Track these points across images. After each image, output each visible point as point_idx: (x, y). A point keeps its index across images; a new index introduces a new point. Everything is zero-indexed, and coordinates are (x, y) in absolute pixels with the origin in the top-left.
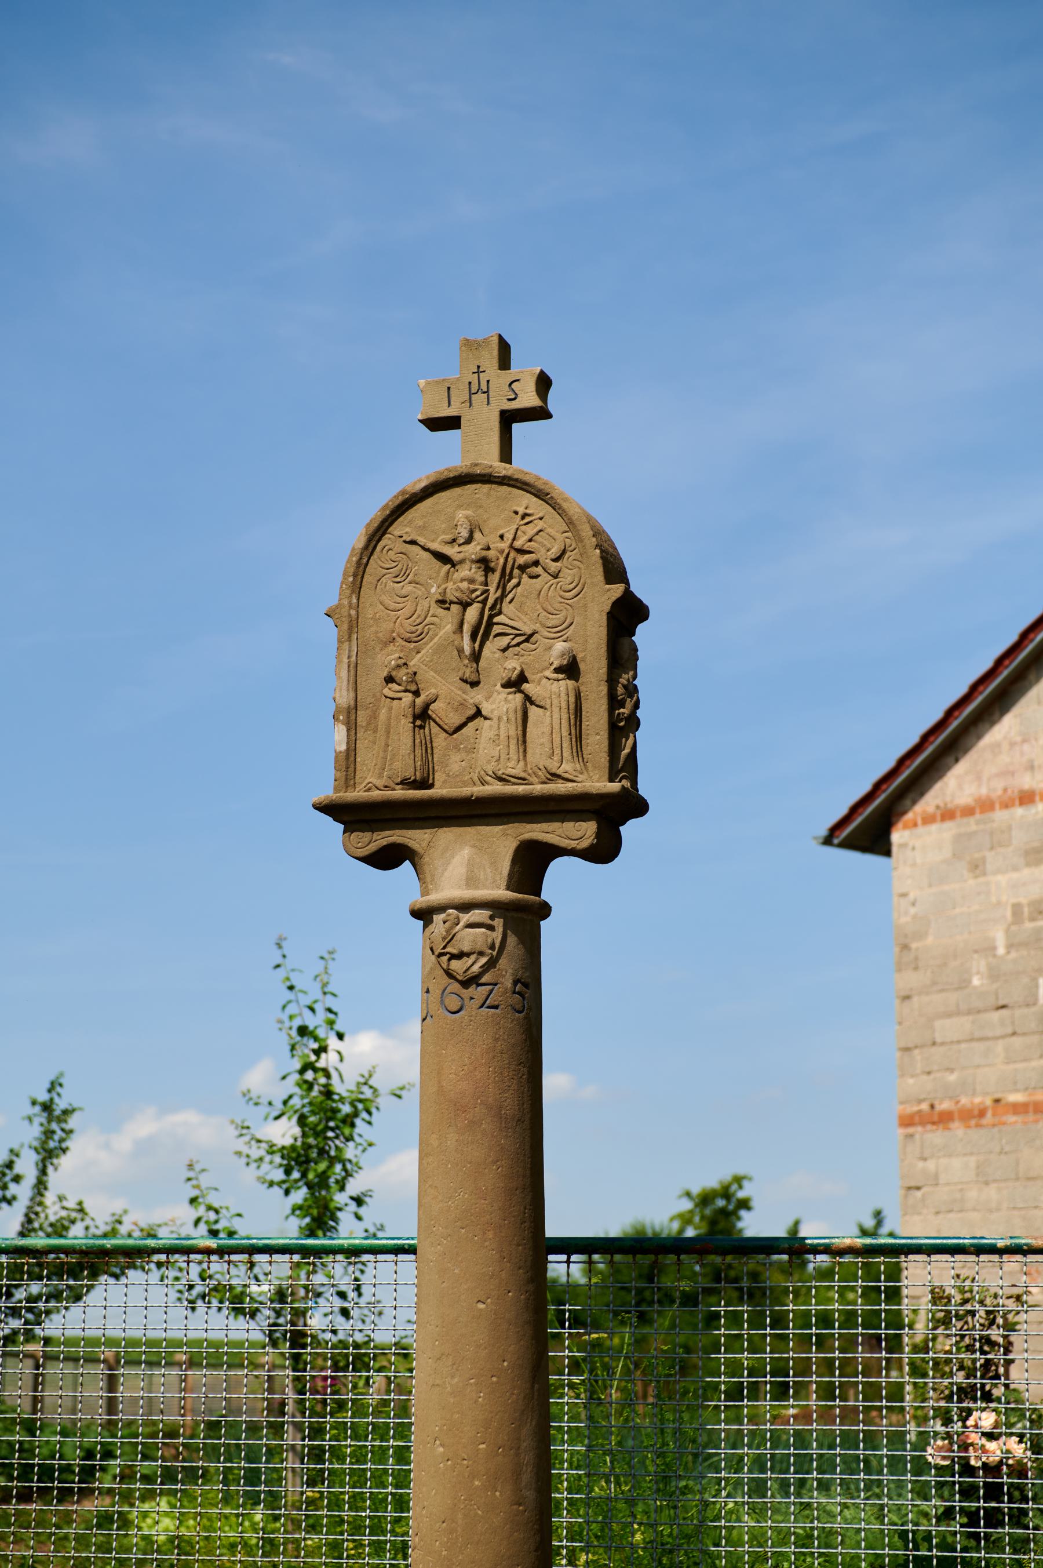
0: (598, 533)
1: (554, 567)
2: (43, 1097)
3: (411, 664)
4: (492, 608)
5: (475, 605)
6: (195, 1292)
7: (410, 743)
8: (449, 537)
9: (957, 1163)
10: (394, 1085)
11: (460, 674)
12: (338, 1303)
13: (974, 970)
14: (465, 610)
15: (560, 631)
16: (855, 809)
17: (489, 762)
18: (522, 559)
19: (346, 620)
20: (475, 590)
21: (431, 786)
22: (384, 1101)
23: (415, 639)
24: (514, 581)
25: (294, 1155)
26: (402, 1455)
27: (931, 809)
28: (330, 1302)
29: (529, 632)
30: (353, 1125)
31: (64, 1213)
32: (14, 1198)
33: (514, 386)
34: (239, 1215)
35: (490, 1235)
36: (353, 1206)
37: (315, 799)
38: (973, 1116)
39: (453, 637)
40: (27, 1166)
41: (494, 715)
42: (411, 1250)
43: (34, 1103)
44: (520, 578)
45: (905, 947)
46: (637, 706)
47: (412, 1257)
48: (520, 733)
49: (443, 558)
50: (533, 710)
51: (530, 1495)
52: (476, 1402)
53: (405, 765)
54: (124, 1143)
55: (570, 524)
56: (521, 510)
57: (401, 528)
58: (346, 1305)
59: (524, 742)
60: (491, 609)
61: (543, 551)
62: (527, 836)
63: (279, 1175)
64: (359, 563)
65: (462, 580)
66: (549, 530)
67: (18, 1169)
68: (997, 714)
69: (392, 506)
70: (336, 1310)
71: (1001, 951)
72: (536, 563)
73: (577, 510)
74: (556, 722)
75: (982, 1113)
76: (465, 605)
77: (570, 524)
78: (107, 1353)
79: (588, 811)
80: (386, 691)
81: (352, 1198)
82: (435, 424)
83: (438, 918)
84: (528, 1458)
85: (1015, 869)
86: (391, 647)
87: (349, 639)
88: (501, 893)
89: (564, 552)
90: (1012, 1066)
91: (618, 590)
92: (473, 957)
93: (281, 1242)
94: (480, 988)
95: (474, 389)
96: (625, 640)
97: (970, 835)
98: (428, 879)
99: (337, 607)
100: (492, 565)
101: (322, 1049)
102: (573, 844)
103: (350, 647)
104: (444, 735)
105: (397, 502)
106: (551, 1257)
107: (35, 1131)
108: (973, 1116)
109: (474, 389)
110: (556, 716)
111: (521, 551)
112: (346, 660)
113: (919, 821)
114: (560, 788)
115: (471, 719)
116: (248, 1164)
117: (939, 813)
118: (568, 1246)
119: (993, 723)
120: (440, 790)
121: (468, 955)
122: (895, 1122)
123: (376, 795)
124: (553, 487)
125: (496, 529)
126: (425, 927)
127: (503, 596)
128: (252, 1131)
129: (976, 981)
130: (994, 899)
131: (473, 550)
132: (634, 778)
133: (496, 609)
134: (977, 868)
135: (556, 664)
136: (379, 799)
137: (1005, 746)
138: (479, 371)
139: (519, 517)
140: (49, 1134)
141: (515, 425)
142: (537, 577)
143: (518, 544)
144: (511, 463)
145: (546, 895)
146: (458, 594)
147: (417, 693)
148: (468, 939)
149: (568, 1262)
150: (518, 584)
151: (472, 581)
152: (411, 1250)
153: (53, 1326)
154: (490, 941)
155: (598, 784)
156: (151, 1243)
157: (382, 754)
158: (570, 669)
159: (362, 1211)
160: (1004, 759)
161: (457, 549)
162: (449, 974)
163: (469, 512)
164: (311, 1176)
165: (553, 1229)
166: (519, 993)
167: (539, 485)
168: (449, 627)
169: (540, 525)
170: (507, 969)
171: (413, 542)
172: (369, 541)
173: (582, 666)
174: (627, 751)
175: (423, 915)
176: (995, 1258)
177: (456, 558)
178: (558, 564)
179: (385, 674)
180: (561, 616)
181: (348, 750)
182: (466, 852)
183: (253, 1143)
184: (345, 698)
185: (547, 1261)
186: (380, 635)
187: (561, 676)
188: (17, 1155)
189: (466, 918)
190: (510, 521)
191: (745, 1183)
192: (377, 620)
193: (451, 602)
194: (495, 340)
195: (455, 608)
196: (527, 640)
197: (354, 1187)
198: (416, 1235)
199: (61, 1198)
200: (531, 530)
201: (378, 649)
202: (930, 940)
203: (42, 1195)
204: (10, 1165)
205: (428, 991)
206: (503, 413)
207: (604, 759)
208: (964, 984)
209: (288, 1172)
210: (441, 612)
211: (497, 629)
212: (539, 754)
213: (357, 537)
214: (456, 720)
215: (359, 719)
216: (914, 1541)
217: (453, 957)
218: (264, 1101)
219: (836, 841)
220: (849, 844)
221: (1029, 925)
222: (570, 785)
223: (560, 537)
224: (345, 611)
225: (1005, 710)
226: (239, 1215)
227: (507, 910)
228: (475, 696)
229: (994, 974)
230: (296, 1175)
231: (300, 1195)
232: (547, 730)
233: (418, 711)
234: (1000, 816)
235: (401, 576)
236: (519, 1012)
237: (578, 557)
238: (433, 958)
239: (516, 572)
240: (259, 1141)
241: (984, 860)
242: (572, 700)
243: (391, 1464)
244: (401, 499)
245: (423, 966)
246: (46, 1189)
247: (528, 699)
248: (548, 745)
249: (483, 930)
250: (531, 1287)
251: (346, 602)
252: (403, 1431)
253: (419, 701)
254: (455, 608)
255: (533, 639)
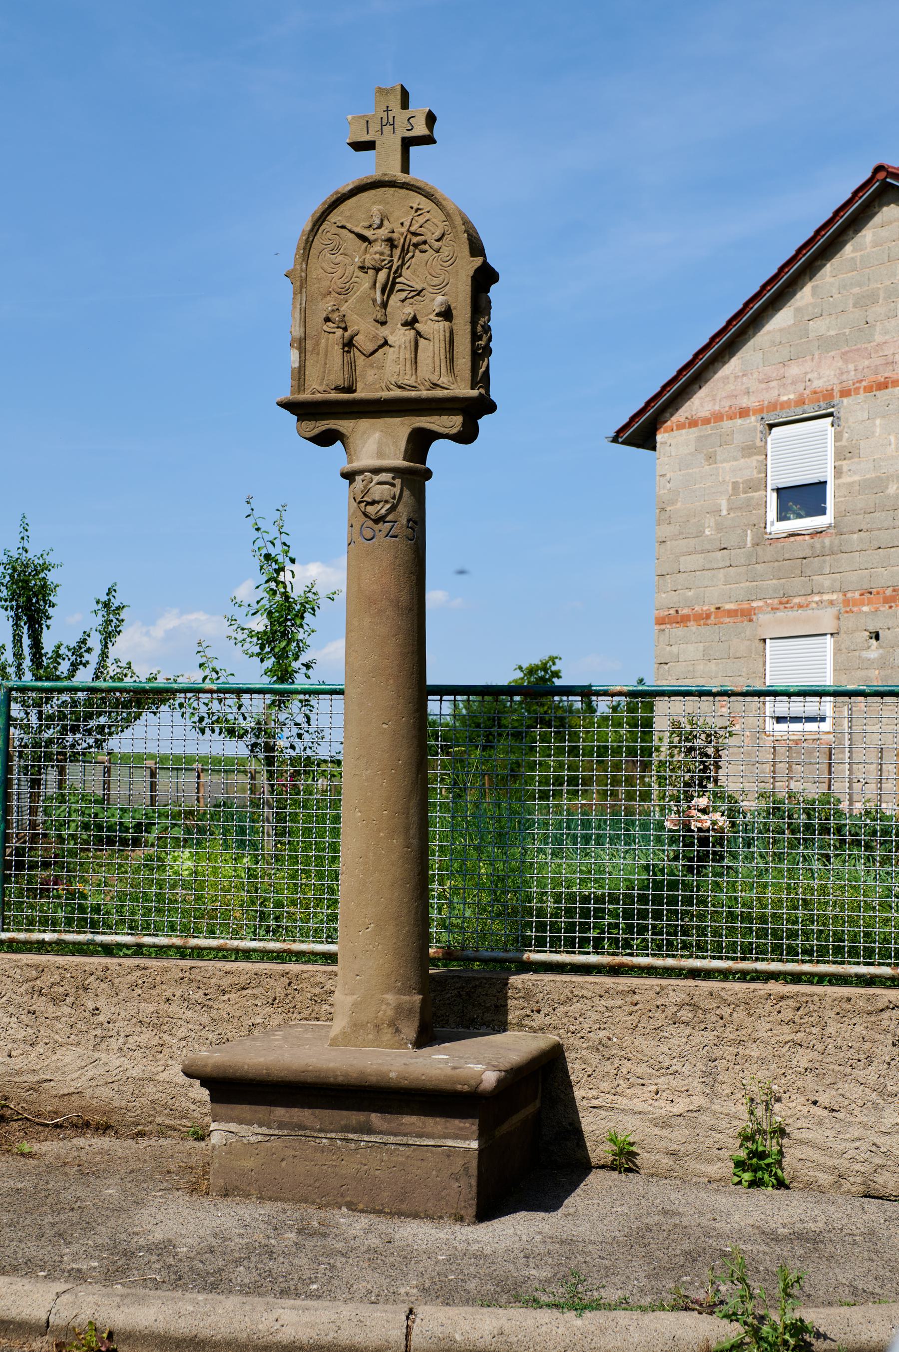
0: (466, 222)
1: (436, 245)
2: (104, 598)
3: (342, 309)
4: (395, 272)
5: (384, 270)
6: (204, 724)
7: (341, 362)
8: (367, 224)
9: (691, 647)
10: (329, 592)
11: (374, 316)
12: (295, 731)
13: (707, 525)
14: (377, 273)
15: (440, 288)
16: (633, 419)
17: (392, 375)
18: (415, 240)
19: (298, 279)
20: (384, 260)
21: (355, 391)
22: (323, 602)
23: (345, 292)
24: (410, 254)
25: (265, 638)
26: (337, 819)
27: (682, 419)
28: (290, 732)
29: (420, 289)
30: (302, 618)
31: (119, 670)
32: (88, 662)
33: (411, 120)
34: (233, 675)
35: (391, 681)
36: (304, 669)
37: (278, 399)
38: (703, 618)
39: (369, 291)
40: (95, 642)
41: (397, 344)
42: (341, 692)
43: (98, 602)
44: (414, 252)
45: (663, 509)
46: (490, 339)
47: (341, 697)
48: (413, 356)
49: (363, 238)
50: (422, 342)
51: (415, 842)
52: (381, 785)
53: (337, 377)
54: (158, 632)
55: (448, 215)
56: (415, 206)
57: (335, 217)
58: (300, 731)
59: (416, 362)
60: (394, 273)
61: (429, 234)
62: (417, 425)
63: (257, 649)
64: (307, 241)
65: (376, 253)
66: (434, 220)
67: (90, 644)
68: (727, 357)
69: (329, 202)
70: (295, 735)
71: (724, 512)
72: (425, 242)
73: (453, 206)
74: (437, 349)
75: (708, 616)
76: (378, 270)
77: (448, 215)
78: (150, 763)
79: (457, 409)
80: (325, 328)
81: (303, 664)
82: (360, 146)
83: (359, 478)
84: (414, 819)
85: (735, 459)
86: (329, 298)
87: (301, 292)
88: (399, 462)
89: (443, 235)
90: (728, 586)
91: (478, 261)
92: (381, 504)
93: (258, 686)
94: (386, 524)
95: (385, 122)
96: (483, 295)
97: (707, 437)
98: (352, 453)
99: (293, 270)
100: (396, 243)
101: (282, 569)
102: (447, 431)
103: (301, 297)
104: (363, 357)
105: (333, 199)
106: (430, 697)
107: (100, 620)
108: (703, 618)
109: (385, 122)
110: (437, 345)
111: (415, 234)
112: (298, 306)
113: (675, 428)
114: (439, 393)
115: (381, 347)
116: (236, 644)
117: (687, 421)
118: (442, 691)
119: (725, 363)
120: (359, 395)
121: (378, 502)
122: (654, 621)
123: (318, 397)
124: (436, 191)
125: (398, 219)
126: (350, 484)
127: (403, 264)
128: (238, 622)
129: (707, 532)
130: (721, 479)
131: (383, 233)
132: (487, 387)
133: (398, 273)
134: (711, 458)
135: (437, 311)
136: (320, 399)
137: (732, 379)
138: (387, 110)
139: (413, 211)
140: (108, 622)
141: (411, 148)
142: (425, 251)
143: (413, 229)
144: (408, 174)
145: (429, 464)
146: (373, 263)
147: (345, 329)
148: (378, 492)
149: (441, 700)
150: (413, 256)
151: (382, 254)
152: (341, 692)
153: (113, 743)
154: (392, 493)
155: (464, 391)
156: (175, 686)
157: (322, 369)
158: (447, 314)
159: (310, 672)
160: (731, 387)
161: (372, 232)
162: (365, 514)
163: (380, 207)
164: (277, 650)
165: (432, 679)
166: (411, 528)
167: (427, 189)
168: (367, 285)
169: (428, 216)
170: (403, 513)
171: (343, 227)
172: (314, 225)
173: (454, 312)
174: (483, 369)
175: (349, 476)
176: (711, 698)
177: (372, 238)
178: (439, 243)
179: (324, 316)
180: (441, 278)
181: (300, 366)
182: (377, 435)
183: (239, 630)
184: (298, 332)
185: (427, 700)
186: (321, 290)
187: (440, 319)
188: (89, 636)
189: (376, 478)
190: (408, 213)
191: (557, 661)
192: (319, 280)
193: (369, 268)
194: (399, 88)
195: (371, 272)
196: (418, 294)
197: (304, 658)
198: (343, 683)
199: (117, 661)
200: (421, 220)
201: (319, 299)
202: (679, 505)
203: (105, 661)
204: (84, 642)
205: (352, 526)
206: (404, 139)
207: (467, 374)
208: (700, 534)
209: (262, 648)
210: (361, 275)
211: (398, 287)
212: (426, 371)
213: (306, 224)
214: (370, 347)
215: (307, 346)
216: (653, 870)
217: (368, 503)
218: (245, 603)
219: (620, 440)
220: (628, 442)
221: (743, 496)
222: (446, 391)
223: (441, 225)
224: (298, 274)
225: (732, 355)
226: (233, 675)
227: (403, 473)
228: (384, 332)
229: (719, 528)
230: (267, 649)
231: (270, 662)
232: (431, 355)
233: (346, 341)
234: (727, 424)
235: (335, 250)
236: (411, 540)
237: (453, 239)
238: (355, 504)
239: (411, 248)
240: (243, 629)
241: (715, 452)
242: (448, 335)
243: (329, 825)
244: (335, 197)
245: (349, 510)
246: (107, 657)
247: (418, 333)
248: (431, 365)
249: (388, 486)
250: (417, 715)
251: (298, 267)
252: (336, 804)
253: (347, 334)
254: (371, 272)
255: (422, 294)
